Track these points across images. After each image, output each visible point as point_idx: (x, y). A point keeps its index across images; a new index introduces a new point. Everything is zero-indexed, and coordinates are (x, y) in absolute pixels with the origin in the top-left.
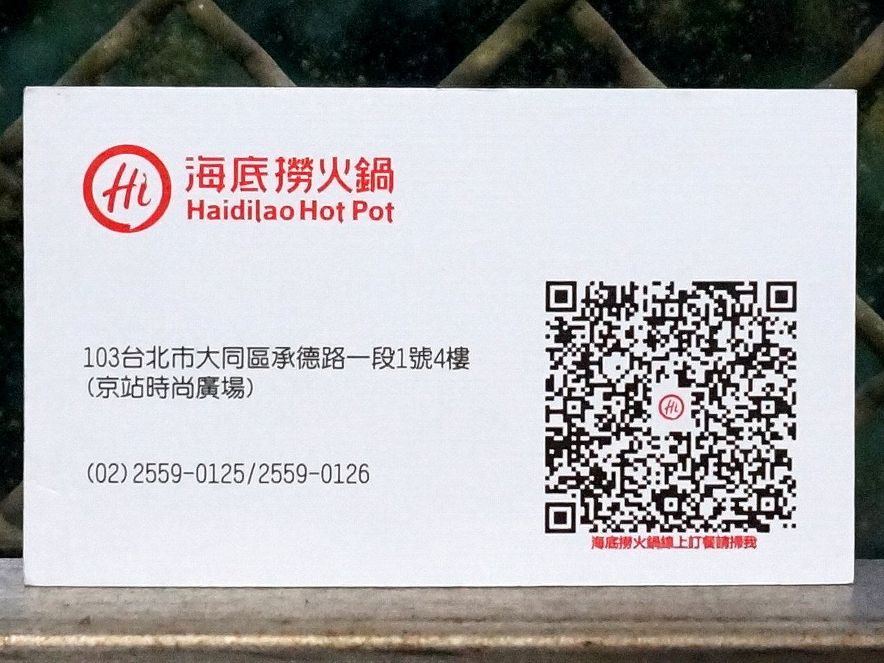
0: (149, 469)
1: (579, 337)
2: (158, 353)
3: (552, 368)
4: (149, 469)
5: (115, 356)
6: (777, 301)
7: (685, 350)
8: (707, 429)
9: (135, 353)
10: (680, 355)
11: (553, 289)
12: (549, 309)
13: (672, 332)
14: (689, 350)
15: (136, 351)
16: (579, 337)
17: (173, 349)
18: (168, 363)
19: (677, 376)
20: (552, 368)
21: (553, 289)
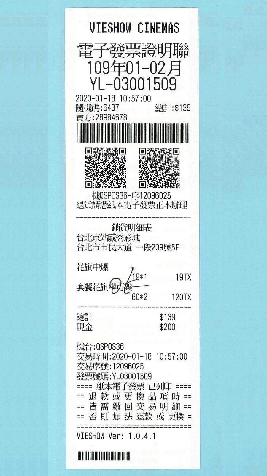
0: (133, 97)
1: (106, 167)
2: (88, 236)
3: (139, 173)
4: (133, 97)
5: (114, 107)
6: (141, 150)
7: (101, 177)
8: (155, 181)
9: (153, 48)
10: (111, 178)
11: (178, 149)
12: (120, 148)
13: (120, 162)
14: (101, 177)
15: (153, 47)
16: (106, 167)
17: (89, 244)
18: (159, 64)
19: (150, 166)
20: (139, 173)
21: (178, 149)
